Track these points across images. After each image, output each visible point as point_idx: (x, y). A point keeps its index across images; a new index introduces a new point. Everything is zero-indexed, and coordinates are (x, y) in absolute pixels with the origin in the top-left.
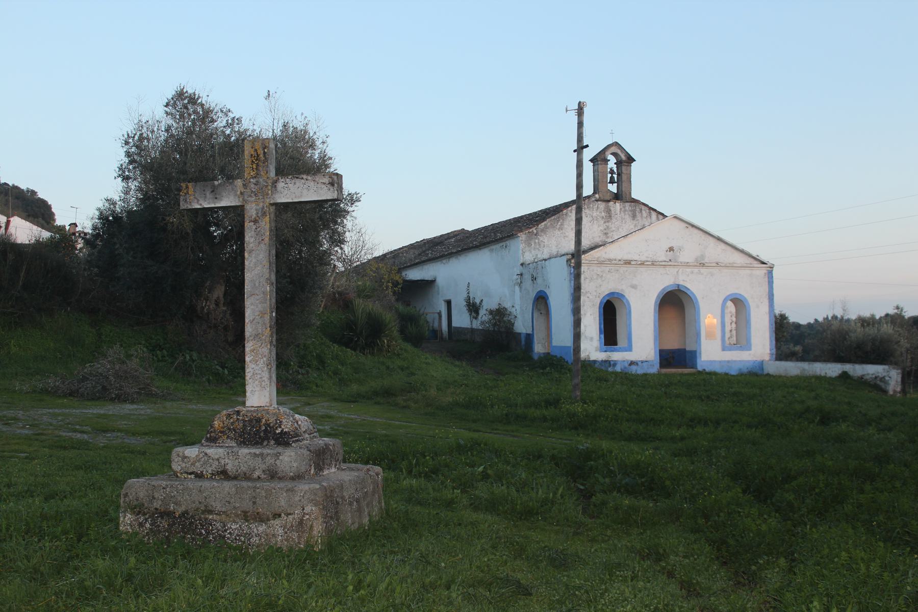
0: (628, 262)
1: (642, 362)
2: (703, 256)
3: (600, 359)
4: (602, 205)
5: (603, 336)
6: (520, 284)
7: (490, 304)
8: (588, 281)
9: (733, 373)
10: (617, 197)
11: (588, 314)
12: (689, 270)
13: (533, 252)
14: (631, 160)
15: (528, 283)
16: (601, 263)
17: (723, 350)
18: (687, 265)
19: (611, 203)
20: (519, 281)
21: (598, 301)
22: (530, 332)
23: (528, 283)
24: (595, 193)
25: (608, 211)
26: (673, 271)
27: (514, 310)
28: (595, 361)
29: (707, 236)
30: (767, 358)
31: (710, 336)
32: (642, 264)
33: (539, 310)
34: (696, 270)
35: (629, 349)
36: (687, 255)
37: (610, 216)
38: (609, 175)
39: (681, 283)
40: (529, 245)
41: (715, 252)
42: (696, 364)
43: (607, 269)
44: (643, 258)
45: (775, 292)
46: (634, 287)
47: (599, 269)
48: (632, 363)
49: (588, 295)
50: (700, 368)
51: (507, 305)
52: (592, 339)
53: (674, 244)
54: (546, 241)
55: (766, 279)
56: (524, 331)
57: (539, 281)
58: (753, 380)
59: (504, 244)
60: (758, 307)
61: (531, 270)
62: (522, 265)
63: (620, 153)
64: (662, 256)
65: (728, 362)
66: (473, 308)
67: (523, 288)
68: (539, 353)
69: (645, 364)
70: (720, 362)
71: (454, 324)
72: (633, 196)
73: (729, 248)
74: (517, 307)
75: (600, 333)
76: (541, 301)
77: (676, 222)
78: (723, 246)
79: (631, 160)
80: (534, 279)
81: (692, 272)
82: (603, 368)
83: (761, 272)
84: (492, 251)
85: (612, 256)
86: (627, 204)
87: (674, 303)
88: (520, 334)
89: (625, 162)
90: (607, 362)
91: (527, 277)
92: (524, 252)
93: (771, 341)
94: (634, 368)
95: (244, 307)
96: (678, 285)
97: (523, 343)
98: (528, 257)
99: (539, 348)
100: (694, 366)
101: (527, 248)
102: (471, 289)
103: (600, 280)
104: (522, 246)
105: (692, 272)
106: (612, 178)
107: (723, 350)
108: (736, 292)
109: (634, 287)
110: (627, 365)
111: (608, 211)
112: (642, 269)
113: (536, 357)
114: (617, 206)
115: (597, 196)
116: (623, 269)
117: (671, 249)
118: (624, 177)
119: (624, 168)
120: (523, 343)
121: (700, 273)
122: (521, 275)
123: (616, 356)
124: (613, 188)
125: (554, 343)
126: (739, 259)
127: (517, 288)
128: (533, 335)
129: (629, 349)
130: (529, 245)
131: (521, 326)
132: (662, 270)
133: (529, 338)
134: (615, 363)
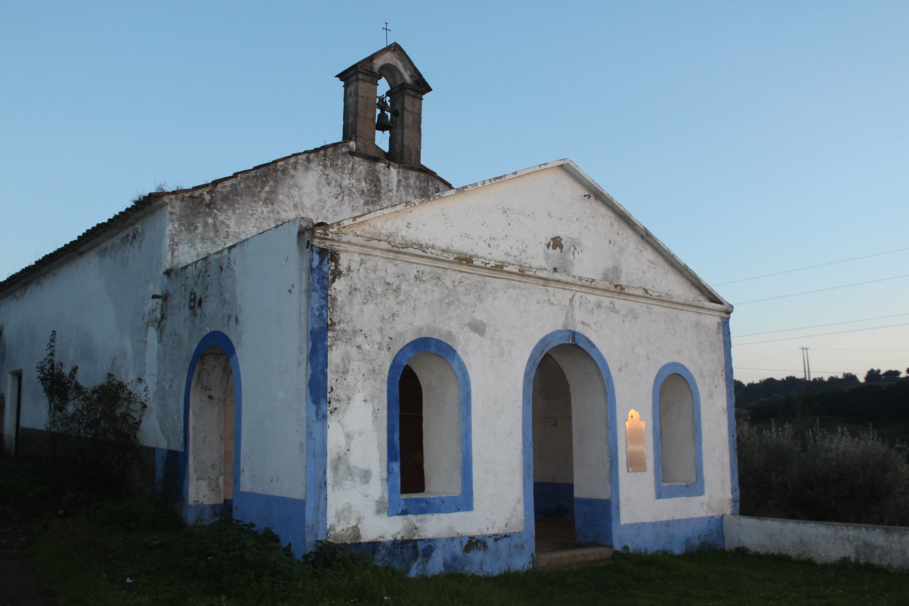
0: (466, 260)
1: (497, 538)
2: (616, 270)
3: (389, 538)
4: (362, 167)
5: (396, 466)
6: (160, 324)
7: (90, 377)
8: (359, 297)
9: (678, 550)
10: (391, 157)
11: (358, 398)
12: (592, 299)
13: (199, 246)
14: (421, 87)
15: (180, 319)
16: (399, 249)
17: (659, 496)
18: (589, 286)
19: (381, 166)
20: (158, 314)
21: (385, 361)
22: (178, 447)
23: (180, 319)
24: (347, 137)
25: (374, 180)
26: (562, 296)
27: (141, 387)
28: (374, 546)
29: (623, 225)
30: (728, 509)
31: (636, 464)
32: (499, 268)
33: (206, 388)
34: (606, 301)
35: (464, 502)
36: (587, 265)
37: (378, 192)
38: (378, 111)
39: (579, 329)
40: (191, 227)
41: (638, 266)
42: (609, 535)
43: (413, 271)
44: (498, 256)
45: (734, 364)
46: (478, 328)
47: (391, 269)
48: (474, 543)
49: (360, 340)
50: (618, 546)
51: (128, 377)
52: (366, 476)
53: (564, 232)
54: (232, 223)
55: (721, 336)
56: (163, 444)
57: (210, 306)
58: (706, 559)
59: (130, 231)
60: (711, 396)
61: (191, 282)
62: (168, 273)
63: (400, 66)
64: (538, 258)
65: (668, 524)
66: (57, 384)
67: (167, 331)
68: (200, 508)
69: (502, 543)
70: (654, 525)
71: (23, 424)
72: (425, 161)
73: (660, 261)
74: (151, 381)
75: (391, 458)
76: (215, 355)
77: (566, 182)
78: (649, 254)
79: (421, 87)
80: (196, 303)
81: (599, 306)
82: (397, 566)
83: (712, 320)
84: (103, 253)
85: (423, 236)
86: (413, 174)
87: (560, 378)
88: (153, 450)
89: (410, 87)
90: (411, 548)
91: (180, 301)
92: (174, 245)
93: (732, 473)
94: (476, 556)
95: (702, 462)
96: (574, 333)
97: (159, 475)
98: (186, 255)
99: (199, 492)
100: (602, 537)
101: (184, 235)
102: (58, 346)
103: (391, 300)
104: (170, 228)
105: (599, 306)
106: (382, 116)
107: (659, 496)
108: (677, 359)
109: (478, 328)
110: (458, 549)
111: (374, 180)
112: (497, 283)
113: (190, 518)
114: (392, 175)
115: (352, 144)
116: (452, 276)
117: (556, 243)
118: (408, 119)
119: (408, 101)
120: (159, 475)
121: (613, 309)
122: (165, 297)
123: (434, 526)
124: (382, 140)
125: (247, 484)
126: (680, 290)
127: (152, 333)
128: (185, 455)
129: (464, 502)
130: (191, 227)
131: (154, 432)
132: (538, 292)
133: (176, 462)
134: (427, 548)
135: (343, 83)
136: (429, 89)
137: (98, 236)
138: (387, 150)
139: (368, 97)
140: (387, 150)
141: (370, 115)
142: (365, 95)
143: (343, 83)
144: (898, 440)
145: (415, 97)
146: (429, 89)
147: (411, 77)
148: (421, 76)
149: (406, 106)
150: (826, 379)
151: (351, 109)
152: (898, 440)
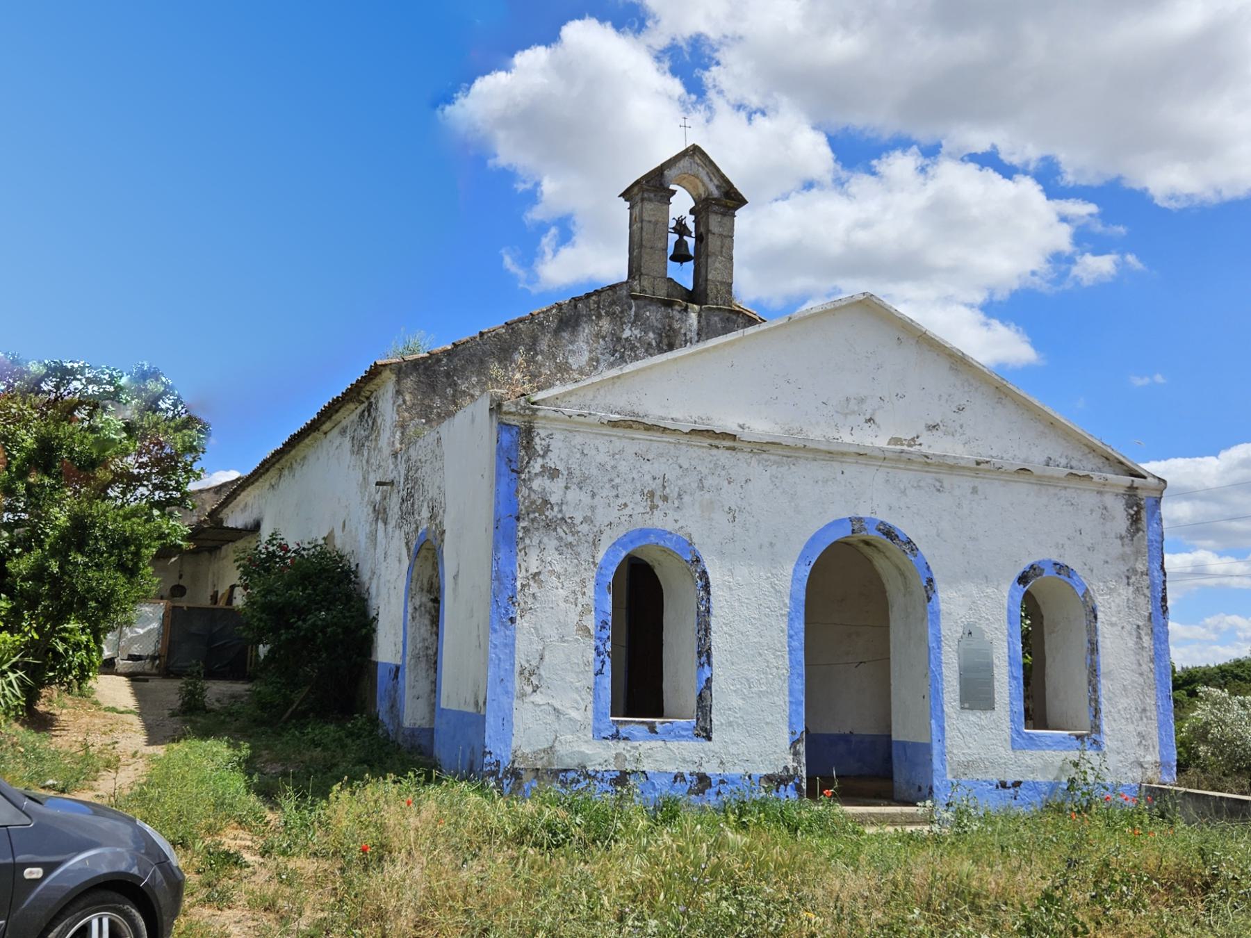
10: (695, 296)
38: (673, 238)
106: (680, 244)
118: (713, 243)
124: (684, 275)
135: (628, 204)
136: (741, 202)
137: (294, 447)
138: (690, 287)
139: (656, 223)
140: (690, 287)
141: (660, 245)
142: (653, 219)
143: (628, 204)
144: (36, 637)
145: (724, 214)
146: (741, 202)
147: (718, 187)
148: (731, 186)
149: (711, 228)
150: (609, 24)
151: (636, 239)
152: (36, 637)
